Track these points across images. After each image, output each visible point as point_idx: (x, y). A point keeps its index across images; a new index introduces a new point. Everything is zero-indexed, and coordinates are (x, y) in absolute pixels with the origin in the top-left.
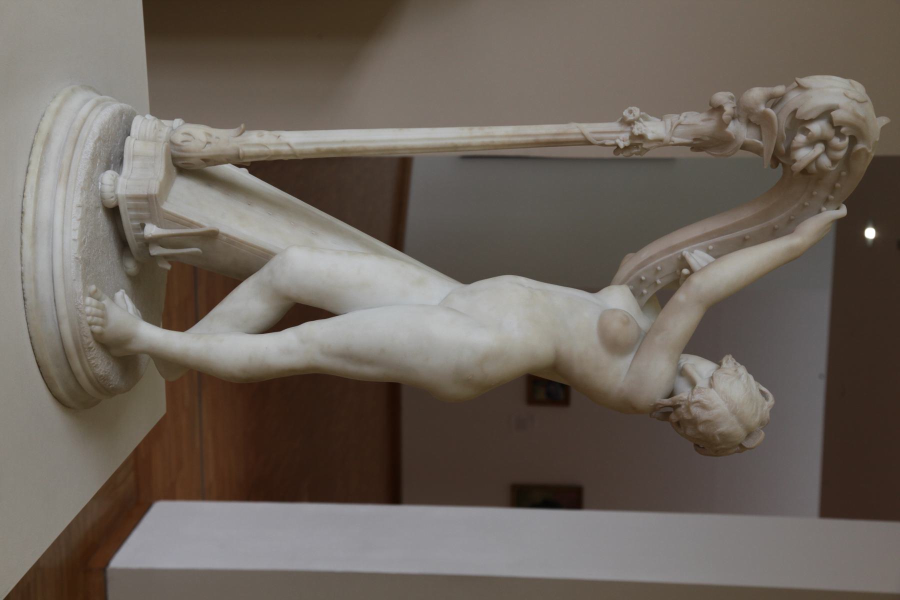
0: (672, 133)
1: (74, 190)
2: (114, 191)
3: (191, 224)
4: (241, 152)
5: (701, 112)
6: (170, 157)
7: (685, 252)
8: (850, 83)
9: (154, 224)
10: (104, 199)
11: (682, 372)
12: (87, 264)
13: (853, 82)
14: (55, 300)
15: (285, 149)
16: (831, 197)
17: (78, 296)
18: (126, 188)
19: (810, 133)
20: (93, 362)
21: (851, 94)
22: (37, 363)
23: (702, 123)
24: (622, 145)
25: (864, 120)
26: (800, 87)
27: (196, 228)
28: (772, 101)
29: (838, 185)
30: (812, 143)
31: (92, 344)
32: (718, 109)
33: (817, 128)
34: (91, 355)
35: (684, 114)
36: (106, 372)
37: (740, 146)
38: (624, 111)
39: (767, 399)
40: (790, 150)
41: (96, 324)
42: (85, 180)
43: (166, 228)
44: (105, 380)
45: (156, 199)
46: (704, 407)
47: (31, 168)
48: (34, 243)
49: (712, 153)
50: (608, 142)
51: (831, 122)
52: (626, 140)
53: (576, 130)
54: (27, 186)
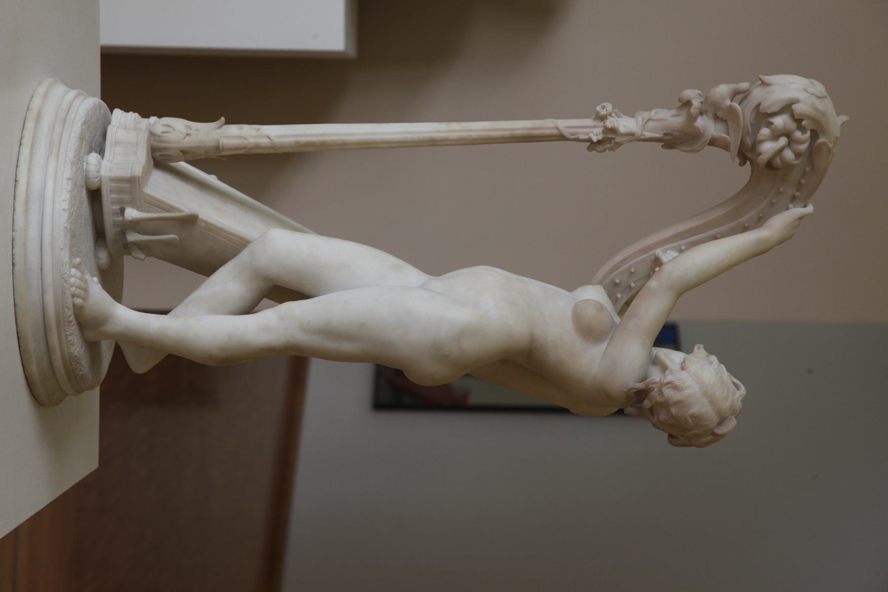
0: (644, 128)
1: (65, 163)
2: (98, 172)
3: (171, 208)
4: (221, 143)
5: (670, 109)
6: (150, 148)
7: (659, 252)
8: (811, 82)
9: (134, 208)
10: (89, 179)
11: (655, 361)
12: (73, 235)
13: (813, 80)
14: (41, 269)
15: (264, 141)
16: (797, 194)
17: (64, 265)
18: (110, 170)
19: (773, 126)
20: (70, 338)
21: (810, 90)
22: (18, 333)
23: (671, 119)
24: (595, 139)
25: (824, 114)
26: (764, 84)
27: (176, 212)
28: (740, 97)
29: (803, 181)
30: (775, 137)
31: (72, 318)
32: (687, 104)
33: (780, 121)
34: (70, 330)
35: (654, 111)
36: (80, 354)
37: (708, 141)
38: (597, 107)
39: (738, 389)
40: (756, 144)
41: (78, 296)
42: (75, 156)
43: (145, 212)
44: (77, 363)
45: (139, 181)
46: (676, 388)
47: (25, 141)
48: (27, 210)
49: (683, 149)
50: (582, 137)
51: (792, 115)
52: (599, 134)
53: (551, 125)
54: (20, 157)
